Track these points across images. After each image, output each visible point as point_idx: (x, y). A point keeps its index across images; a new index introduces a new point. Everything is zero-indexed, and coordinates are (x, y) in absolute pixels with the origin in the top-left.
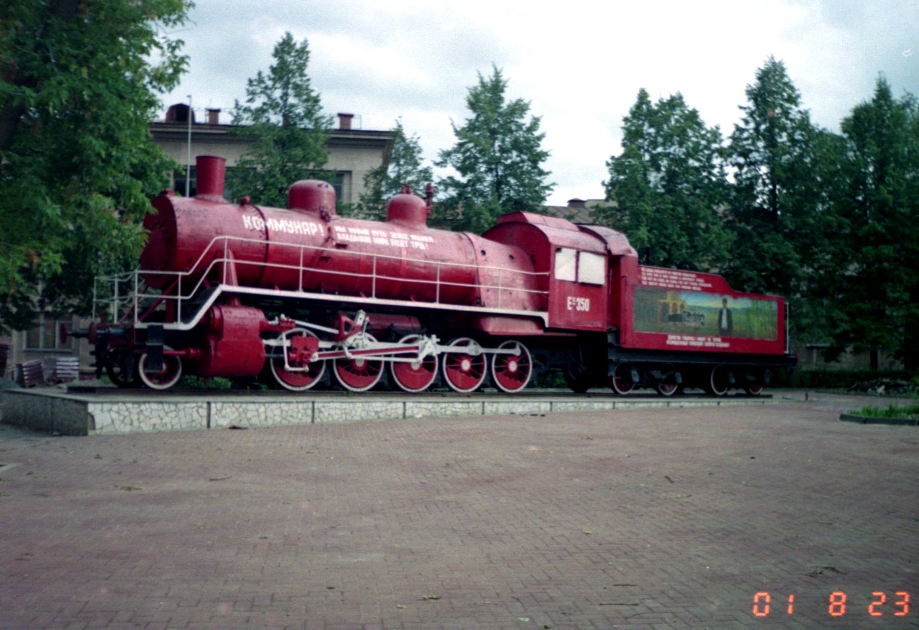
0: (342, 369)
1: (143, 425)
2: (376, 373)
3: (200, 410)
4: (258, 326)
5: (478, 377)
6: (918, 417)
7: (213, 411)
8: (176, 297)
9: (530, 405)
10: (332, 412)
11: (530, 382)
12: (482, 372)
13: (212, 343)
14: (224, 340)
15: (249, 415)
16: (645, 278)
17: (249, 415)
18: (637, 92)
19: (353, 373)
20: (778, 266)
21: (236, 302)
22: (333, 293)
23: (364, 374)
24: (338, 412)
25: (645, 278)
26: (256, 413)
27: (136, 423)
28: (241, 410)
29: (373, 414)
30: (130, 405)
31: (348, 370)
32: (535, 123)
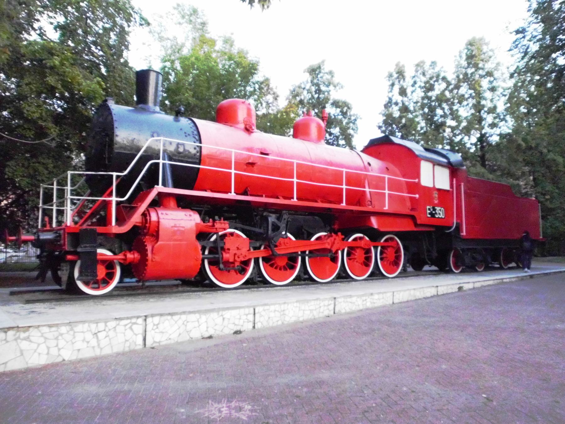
0: (214, 268)
1: (62, 352)
2: (293, 268)
3: (134, 327)
4: (195, 228)
6: (4, 374)
7: (149, 328)
8: (55, 205)
9: (312, 305)
10: (272, 315)
11: (297, 276)
12: (371, 262)
13: (149, 248)
14: (159, 243)
15: (190, 326)
16: (57, 130)
19: (276, 268)
20: (328, 130)
22: (453, 205)
23: (285, 269)
24: (278, 314)
25: (57, 130)
26: (196, 324)
27: (54, 351)
28: (180, 322)
29: (308, 312)
30: (45, 329)
31: (272, 266)
32: (228, 41)
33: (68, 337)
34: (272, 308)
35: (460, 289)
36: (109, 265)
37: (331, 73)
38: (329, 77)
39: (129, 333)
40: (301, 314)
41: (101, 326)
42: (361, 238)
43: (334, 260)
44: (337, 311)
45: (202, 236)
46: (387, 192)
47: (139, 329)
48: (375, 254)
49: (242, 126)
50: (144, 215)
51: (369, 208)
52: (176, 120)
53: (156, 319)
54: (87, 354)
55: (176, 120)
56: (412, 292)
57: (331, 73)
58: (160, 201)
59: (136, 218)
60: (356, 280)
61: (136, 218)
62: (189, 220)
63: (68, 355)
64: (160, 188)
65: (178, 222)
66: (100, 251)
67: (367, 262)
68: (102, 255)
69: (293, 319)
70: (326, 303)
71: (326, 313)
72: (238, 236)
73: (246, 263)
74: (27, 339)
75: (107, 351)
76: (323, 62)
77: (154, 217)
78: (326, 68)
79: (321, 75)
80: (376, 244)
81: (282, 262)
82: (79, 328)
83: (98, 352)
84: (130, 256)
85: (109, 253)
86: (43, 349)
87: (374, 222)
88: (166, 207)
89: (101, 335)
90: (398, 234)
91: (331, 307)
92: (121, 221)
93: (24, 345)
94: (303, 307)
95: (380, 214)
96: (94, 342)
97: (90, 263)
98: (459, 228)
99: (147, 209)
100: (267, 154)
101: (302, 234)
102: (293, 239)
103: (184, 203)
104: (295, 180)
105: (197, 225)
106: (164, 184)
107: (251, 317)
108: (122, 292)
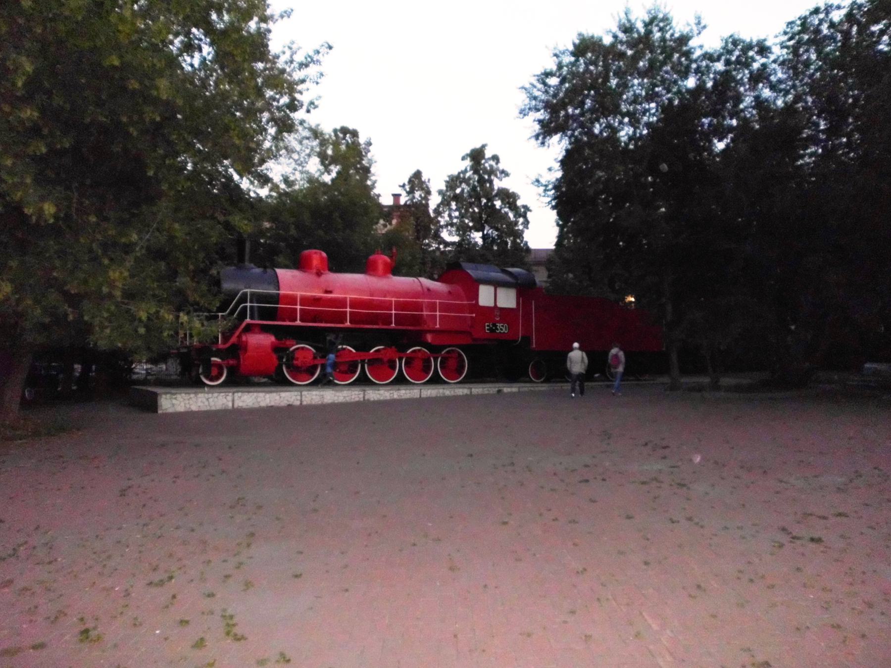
2: (355, 372)
5: (428, 373)
7: (236, 398)
12: (357, 368)
15: (259, 400)
17: (259, 400)
18: (412, 172)
21: (256, 330)
23: (346, 372)
33: (194, 399)
34: (314, 393)
35: (499, 391)
36: (220, 367)
37: (496, 158)
38: (493, 163)
39: (225, 401)
40: (336, 398)
41: (210, 395)
42: (419, 350)
43: (393, 368)
44: (366, 398)
45: (276, 349)
46: (438, 313)
47: (230, 398)
48: (435, 365)
49: (315, 271)
50: (239, 337)
51: (426, 327)
52: (265, 272)
53: (240, 394)
54: (204, 409)
55: (265, 272)
56: (441, 391)
57: (496, 158)
58: (249, 329)
59: (234, 339)
60: (414, 384)
61: (234, 339)
62: (265, 340)
63: (194, 408)
64: (248, 320)
65: (261, 341)
66: (213, 359)
67: (427, 369)
68: (870, 369)
69: (330, 401)
70: (357, 393)
71: (357, 399)
72: (308, 349)
73: (315, 368)
74: (176, 399)
75: (213, 408)
76: (484, 146)
77: (244, 338)
78: (488, 154)
79: (483, 161)
80: (435, 355)
81: (344, 368)
82: (200, 395)
83: (208, 408)
84: (231, 362)
85: (218, 360)
86: (182, 404)
87: (429, 338)
88: (254, 333)
89: (211, 400)
90: (460, 347)
91: (361, 396)
92: (224, 342)
93: (174, 401)
94: (338, 394)
95: (433, 331)
96: (207, 403)
97: (208, 365)
98: (527, 339)
99: (240, 333)
100: (330, 292)
101: (363, 347)
102: (354, 351)
103: (264, 329)
104: (298, 307)
105: (272, 343)
106: (252, 318)
107: (299, 398)
108: (225, 385)
